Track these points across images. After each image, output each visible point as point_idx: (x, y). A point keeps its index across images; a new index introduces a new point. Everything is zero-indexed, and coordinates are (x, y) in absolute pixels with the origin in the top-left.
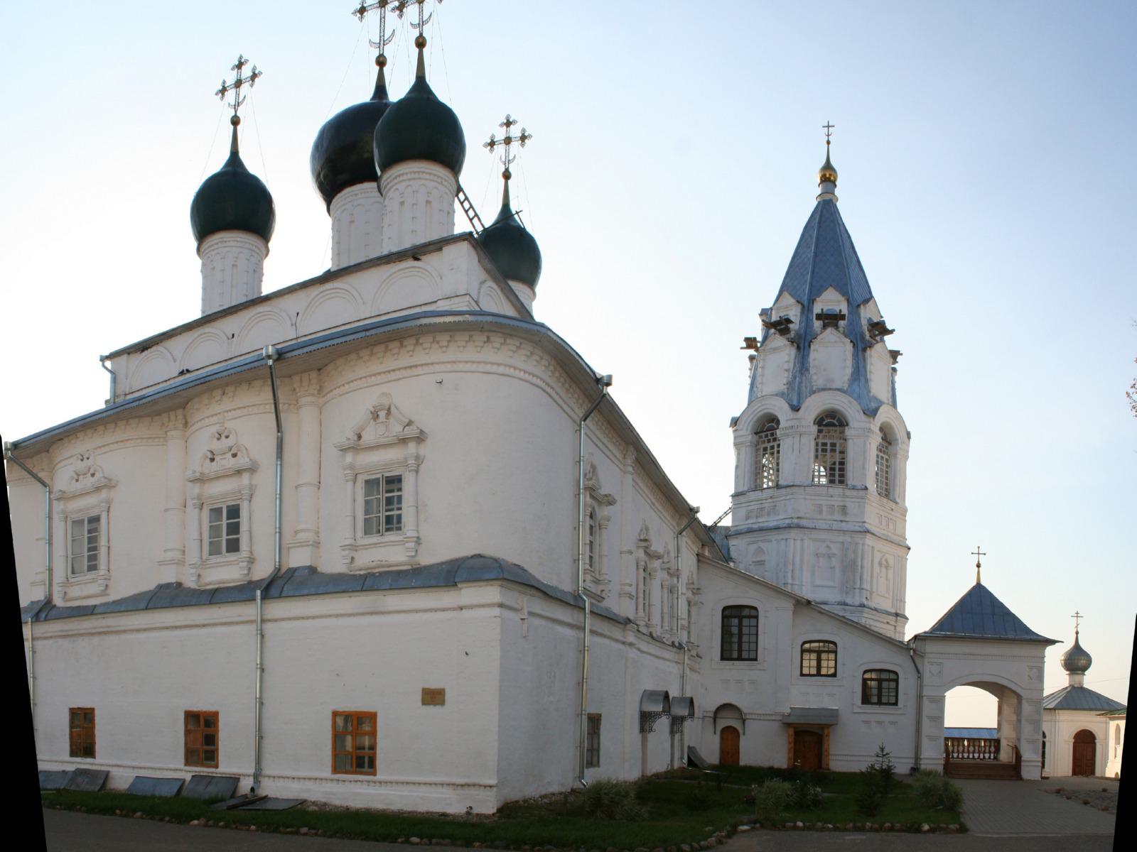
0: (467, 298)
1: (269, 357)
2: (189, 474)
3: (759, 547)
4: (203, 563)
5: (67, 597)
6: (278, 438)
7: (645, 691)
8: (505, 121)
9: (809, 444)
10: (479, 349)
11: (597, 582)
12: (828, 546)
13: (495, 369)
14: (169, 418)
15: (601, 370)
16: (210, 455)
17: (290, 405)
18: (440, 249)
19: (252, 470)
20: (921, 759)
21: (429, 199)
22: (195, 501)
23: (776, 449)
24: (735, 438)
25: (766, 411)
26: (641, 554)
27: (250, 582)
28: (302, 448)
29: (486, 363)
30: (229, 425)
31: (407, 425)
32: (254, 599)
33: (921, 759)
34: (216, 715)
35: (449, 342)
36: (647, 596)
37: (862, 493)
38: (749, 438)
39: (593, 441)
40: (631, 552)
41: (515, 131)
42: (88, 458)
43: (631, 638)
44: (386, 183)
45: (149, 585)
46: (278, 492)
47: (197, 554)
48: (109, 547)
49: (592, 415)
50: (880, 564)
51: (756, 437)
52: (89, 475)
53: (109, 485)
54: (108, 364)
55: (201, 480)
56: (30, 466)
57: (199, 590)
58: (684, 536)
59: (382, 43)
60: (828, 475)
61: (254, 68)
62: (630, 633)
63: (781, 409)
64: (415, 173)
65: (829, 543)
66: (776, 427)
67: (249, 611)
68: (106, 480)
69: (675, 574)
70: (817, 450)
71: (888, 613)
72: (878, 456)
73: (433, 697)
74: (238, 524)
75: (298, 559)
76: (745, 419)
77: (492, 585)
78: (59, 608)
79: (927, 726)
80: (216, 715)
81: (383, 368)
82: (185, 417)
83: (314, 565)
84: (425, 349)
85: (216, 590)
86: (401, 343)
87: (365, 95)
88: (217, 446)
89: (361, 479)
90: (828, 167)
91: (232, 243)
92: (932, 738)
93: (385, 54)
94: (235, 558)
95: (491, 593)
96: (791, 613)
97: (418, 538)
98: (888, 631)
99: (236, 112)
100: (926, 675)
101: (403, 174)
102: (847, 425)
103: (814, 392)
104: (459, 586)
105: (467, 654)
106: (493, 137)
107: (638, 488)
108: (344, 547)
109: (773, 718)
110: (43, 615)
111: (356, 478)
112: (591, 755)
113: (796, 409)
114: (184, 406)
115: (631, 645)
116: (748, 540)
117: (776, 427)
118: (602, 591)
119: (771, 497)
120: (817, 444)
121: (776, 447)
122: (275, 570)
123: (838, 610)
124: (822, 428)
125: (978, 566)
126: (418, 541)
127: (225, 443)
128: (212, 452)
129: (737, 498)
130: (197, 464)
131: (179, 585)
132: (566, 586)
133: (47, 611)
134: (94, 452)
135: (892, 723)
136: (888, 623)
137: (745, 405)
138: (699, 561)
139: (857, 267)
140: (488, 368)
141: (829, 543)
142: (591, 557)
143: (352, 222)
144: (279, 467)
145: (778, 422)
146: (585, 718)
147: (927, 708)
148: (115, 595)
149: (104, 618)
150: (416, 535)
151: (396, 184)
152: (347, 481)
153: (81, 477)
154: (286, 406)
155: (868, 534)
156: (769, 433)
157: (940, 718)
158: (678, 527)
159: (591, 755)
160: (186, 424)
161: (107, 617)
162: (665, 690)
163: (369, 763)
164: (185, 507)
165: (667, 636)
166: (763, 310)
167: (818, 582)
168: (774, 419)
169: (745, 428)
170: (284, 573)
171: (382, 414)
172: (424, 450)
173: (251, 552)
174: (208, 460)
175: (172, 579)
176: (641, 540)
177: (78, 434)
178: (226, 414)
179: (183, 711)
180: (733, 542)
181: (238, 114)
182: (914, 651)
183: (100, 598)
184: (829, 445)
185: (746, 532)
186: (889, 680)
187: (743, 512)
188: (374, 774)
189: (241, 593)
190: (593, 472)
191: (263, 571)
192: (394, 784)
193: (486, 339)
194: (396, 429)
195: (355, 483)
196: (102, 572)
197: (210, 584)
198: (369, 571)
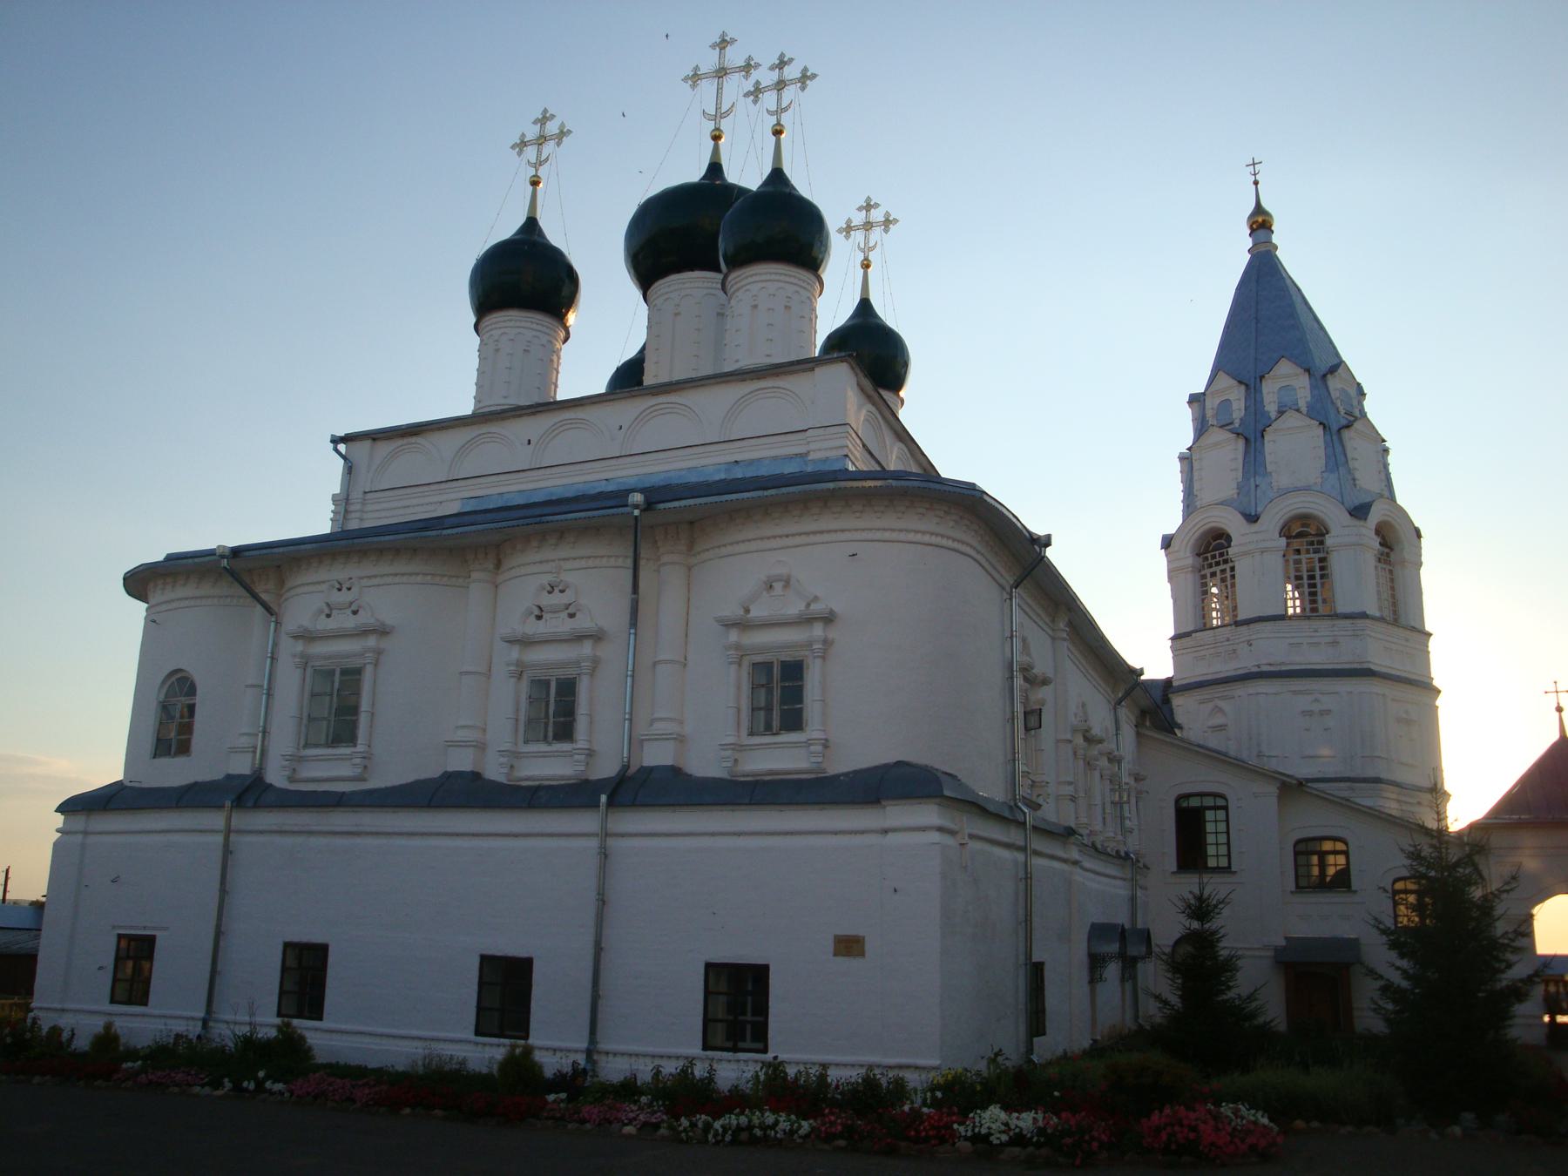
1: (636, 506)
3: (1217, 707)
6: (632, 599)
9: (1275, 562)
13: (919, 537)
15: (1037, 527)
16: (537, 612)
18: (812, 369)
19: (597, 637)
21: (788, 304)
22: (512, 668)
23: (1228, 574)
27: (586, 783)
29: (908, 531)
30: (568, 577)
32: (596, 805)
38: (1189, 560)
39: (986, 570)
42: (349, 589)
43: (1075, 854)
44: (733, 282)
46: (630, 667)
49: (1025, 582)
52: (349, 612)
54: (342, 447)
55: (526, 642)
58: (1123, 706)
59: (719, 115)
61: (563, 125)
63: (1233, 523)
66: (1226, 545)
67: (587, 821)
69: (1115, 760)
72: (1376, 567)
73: (849, 946)
75: (656, 756)
81: (778, 531)
85: (538, 788)
87: (694, 173)
88: (547, 600)
89: (746, 662)
90: (1259, 209)
91: (516, 323)
95: (927, 814)
96: (1275, 800)
97: (826, 740)
99: (536, 171)
104: (883, 803)
105: (895, 891)
108: (724, 746)
112: (1036, 1022)
113: (1252, 518)
115: (1076, 863)
116: (1198, 698)
117: (1226, 545)
118: (1039, 795)
120: (1287, 561)
121: (1228, 570)
127: (557, 599)
130: (514, 620)
138: (1138, 734)
139: (1299, 295)
143: (677, 314)
144: (632, 637)
145: (1229, 539)
148: (375, 783)
150: (823, 737)
151: (749, 284)
152: (731, 663)
153: (334, 612)
156: (1209, 555)
159: (1036, 1022)
166: (1191, 395)
168: (1223, 534)
171: (778, 586)
172: (833, 633)
175: (669, 762)
180: (1177, 701)
191: (606, 769)
194: (794, 608)
196: (360, 748)
197: (527, 779)
198: (758, 778)
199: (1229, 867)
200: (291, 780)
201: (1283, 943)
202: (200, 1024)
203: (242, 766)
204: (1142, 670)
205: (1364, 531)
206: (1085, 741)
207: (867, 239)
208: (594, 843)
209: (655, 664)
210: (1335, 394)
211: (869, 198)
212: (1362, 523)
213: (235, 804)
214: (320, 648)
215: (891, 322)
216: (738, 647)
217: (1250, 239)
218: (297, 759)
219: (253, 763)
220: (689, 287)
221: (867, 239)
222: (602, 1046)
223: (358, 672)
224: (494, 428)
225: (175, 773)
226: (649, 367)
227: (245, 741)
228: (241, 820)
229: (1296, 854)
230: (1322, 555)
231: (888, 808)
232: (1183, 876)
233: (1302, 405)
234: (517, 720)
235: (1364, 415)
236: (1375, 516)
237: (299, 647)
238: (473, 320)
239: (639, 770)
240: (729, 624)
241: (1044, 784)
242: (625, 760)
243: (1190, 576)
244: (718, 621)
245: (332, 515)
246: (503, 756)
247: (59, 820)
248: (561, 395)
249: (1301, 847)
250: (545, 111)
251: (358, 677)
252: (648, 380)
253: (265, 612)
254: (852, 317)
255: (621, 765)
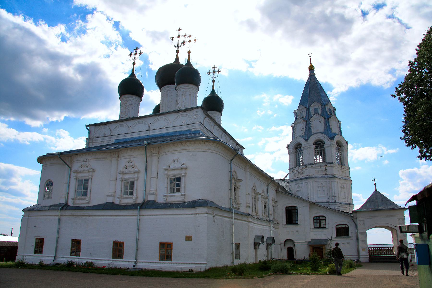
0: (200, 124)
1: (146, 144)
2: (119, 171)
3: (299, 185)
4: (121, 197)
5: (74, 203)
6: (146, 164)
7: (256, 236)
8: (213, 67)
9: (312, 151)
10: (202, 146)
11: (237, 204)
12: (321, 183)
14: (113, 154)
16: (126, 167)
17: (150, 155)
19: (138, 172)
20: (360, 256)
24: (288, 151)
25: (298, 142)
26: (254, 194)
27: (136, 204)
28: (153, 167)
31: (182, 165)
32: (137, 209)
33: (360, 256)
34: (123, 243)
35: (194, 144)
36: (256, 206)
37: (332, 165)
38: (293, 151)
40: (249, 194)
41: (216, 70)
42: (86, 162)
43: (250, 220)
45: (103, 202)
47: (120, 194)
48: (91, 189)
50: (341, 188)
51: (295, 150)
52: (86, 167)
53: (93, 171)
54: (88, 128)
55: (123, 173)
56: (64, 160)
57: (120, 205)
60: (323, 158)
61: (141, 51)
62: (250, 218)
63: (302, 141)
64: (186, 87)
65: (322, 182)
67: (135, 212)
68: (92, 170)
70: (315, 153)
71: (346, 204)
73: (189, 238)
74: (133, 187)
75: (151, 198)
76: (291, 145)
77: (205, 208)
78: (70, 206)
79: (361, 244)
80: (123, 243)
82: (118, 154)
83: (155, 200)
84: (188, 145)
85: (125, 205)
86: (182, 144)
87: (171, 61)
88: (128, 164)
91: (132, 98)
92: (364, 249)
93: (179, 50)
94: (132, 197)
98: (346, 210)
99: (134, 61)
100: (359, 227)
101: (184, 87)
102: (325, 143)
103: (313, 135)
106: (210, 71)
107: (251, 174)
108: (164, 196)
109: (305, 243)
110: (65, 208)
111: (168, 177)
113: (307, 140)
114: (118, 152)
119: (301, 169)
120: (315, 151)
121: (302, 153)
122: (143, 201)
123: (326, 205)
124: (316, 145)
125: (375, 184)
126: (185, 195)
127: (131, 164)
128: (126, 166)
129: (290, 170)
131: (113, 203)
132: (227, 206)
133: (66, 207)
134: (88, 160)
135: (348, 243)
136: (346, 207)
137: (291, 140)
140: (204, 150)
141: (322, 182)
142: (235, 197)
144: (146, 172)
146: (234, 245)
147: (360, 236)
148: (92, 204)
149: (87, 211)
150: (184, 194)
152: (166, 178)
153: (83, 167)
154: (149, 156)
155: (335, 178)
156: (299, 149)
157: (365, 241)
158: (267, 183)
160: (118, 157)
161: (88, 211)
162: (262, 235)
163: (170, 257)
164: (116, 180)
165: (264, 218)
167: (319, 196)
169: (291, 148)
170: (146, 202)
171: (176, 161)
173: (137, 195)
174: (125, 168)
175: (111, 201)
176: (253, 190)
177: (84, 154)
178: (131, 156)
179: (113, 241)
181: (135, 62)
182: (353, 217)
183: (87, 205)
184: (319, 150)
185: (294, 181)
186: (323, 219)
187: (292, 174)
188: (172, 261)
189: (133, 207)
190: (235, 173)
191: (140, 201)
192: (179, 264)
193: (204, 143)
195: (168, 178)
196: (88, 197)
199: (298, 223)
200: (73, 203)
201: (310, 241)
202: (54, 258)
203: (63, 201)
204: (273, 177)
205: (333, 143)
206: (254, 194)
207: (214, 75)
208: (137, 217)
209: (151, 178)
210: (327, 110)
211: (214, 66)
212: (332, 141)
213: (61, 209)
214: (80, 175)
215: (219, 95)
216: (167, 174)
217: (309, 72)
218: (75, 199)
219: (65, 200)
220: (171, 88)
221: (214, 75)
222: (139, 261)
223: (88, 180)
224: (123, 123)
225: (49, 203)
226: (161, 109)
227: (64, 196)
228: (63, 212)
229: (314, 220)
230: (323, 149)
231: (197, 209)
232: (288, 225)
233: (320, 113)
234: (121, 191)
235: (335, 114)
236: (336, 138)
237: (75, 175)
238: (119, 97)
239: (147, 201)
240: (165, 170)
241: (240, 204)
242: (144, 199)
243: (293, 154)
244: (163, 169)
245: (86, 143)
246: (164, 197)
247: (23, 213)
248: (140, 115)
249: (315, 218)
250: (137, 47)
251: (88, 181)
252: (161, 111)
253: (68, 167)
254: (210, 94)
255: (143, 200)
